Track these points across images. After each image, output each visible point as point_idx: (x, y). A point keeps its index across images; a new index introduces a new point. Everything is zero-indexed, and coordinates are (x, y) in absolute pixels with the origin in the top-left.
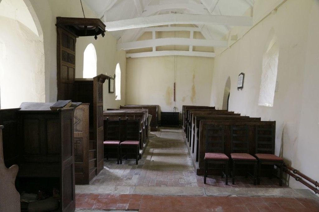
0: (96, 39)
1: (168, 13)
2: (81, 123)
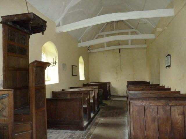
0: (43, 35)
1: (103, 37)
2: (7, 108)
